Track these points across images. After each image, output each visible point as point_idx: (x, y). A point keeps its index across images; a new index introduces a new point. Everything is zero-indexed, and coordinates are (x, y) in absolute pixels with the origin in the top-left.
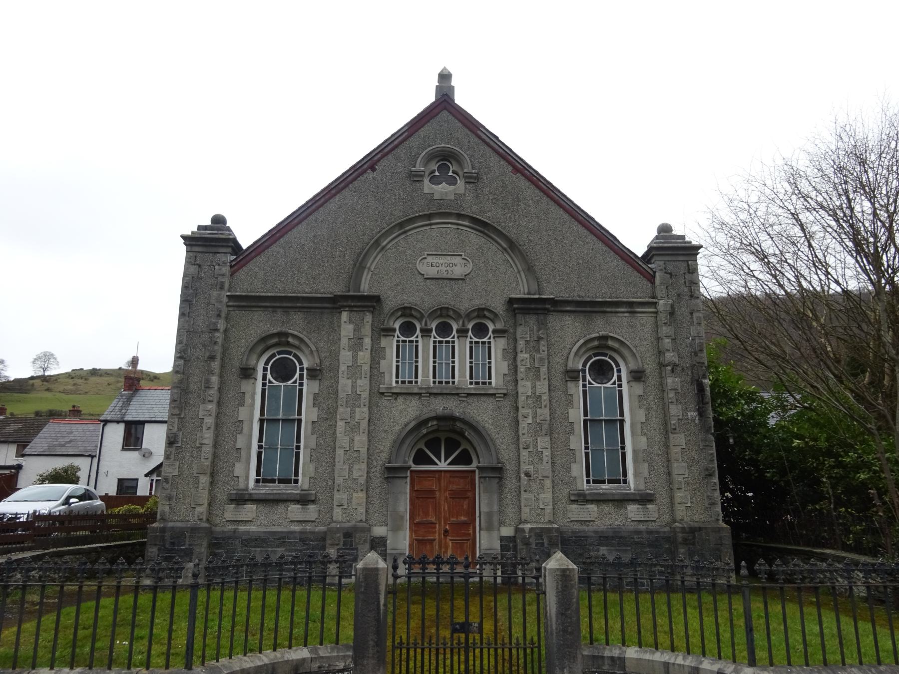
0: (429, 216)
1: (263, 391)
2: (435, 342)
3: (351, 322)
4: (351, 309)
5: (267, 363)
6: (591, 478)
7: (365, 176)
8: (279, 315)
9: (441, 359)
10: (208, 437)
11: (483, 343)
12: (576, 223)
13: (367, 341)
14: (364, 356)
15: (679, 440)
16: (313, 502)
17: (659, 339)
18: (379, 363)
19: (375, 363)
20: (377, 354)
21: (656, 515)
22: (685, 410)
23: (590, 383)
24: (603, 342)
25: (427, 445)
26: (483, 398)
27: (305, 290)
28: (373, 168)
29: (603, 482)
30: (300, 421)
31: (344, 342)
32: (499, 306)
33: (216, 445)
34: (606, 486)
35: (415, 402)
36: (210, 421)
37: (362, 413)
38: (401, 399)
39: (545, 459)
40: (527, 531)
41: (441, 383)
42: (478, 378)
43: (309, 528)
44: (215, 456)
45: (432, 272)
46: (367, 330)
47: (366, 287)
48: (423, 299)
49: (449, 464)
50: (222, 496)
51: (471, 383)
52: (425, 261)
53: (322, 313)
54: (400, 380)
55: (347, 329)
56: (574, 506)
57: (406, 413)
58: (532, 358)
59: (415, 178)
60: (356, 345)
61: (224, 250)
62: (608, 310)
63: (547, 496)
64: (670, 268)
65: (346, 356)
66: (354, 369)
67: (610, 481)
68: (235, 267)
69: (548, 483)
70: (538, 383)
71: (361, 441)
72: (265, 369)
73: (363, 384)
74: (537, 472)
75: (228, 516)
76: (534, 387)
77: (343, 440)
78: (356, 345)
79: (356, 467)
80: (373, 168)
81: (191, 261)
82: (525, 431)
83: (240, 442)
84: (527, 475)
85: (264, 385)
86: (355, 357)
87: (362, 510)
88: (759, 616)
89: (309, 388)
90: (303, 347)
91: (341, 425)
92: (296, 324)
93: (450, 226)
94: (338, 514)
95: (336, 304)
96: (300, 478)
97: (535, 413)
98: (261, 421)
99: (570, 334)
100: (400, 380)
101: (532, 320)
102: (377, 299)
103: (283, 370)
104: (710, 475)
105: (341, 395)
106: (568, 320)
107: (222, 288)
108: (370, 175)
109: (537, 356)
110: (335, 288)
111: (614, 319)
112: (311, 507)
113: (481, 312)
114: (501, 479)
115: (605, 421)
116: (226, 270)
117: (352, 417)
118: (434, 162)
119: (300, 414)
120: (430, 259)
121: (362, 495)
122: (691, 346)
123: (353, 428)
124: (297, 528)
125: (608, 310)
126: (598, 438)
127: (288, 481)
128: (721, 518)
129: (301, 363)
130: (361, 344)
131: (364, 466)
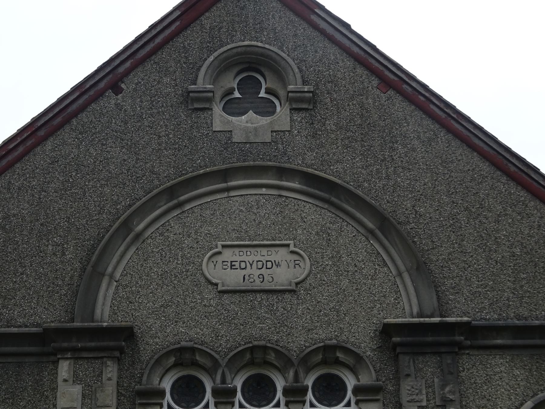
0: (225, 174)
3: (76, 379)
7: (102, 102)
12: (504, 179)
28: (116, 89)
45: (232, 279)
47: (105, 310)
52: (220, 259)
80: (116, 89)
93: (264, 191)
106: (499, 364)
108: (110, 101)
110: (47, 315)
113: (330, 354)
120: (228, 255)
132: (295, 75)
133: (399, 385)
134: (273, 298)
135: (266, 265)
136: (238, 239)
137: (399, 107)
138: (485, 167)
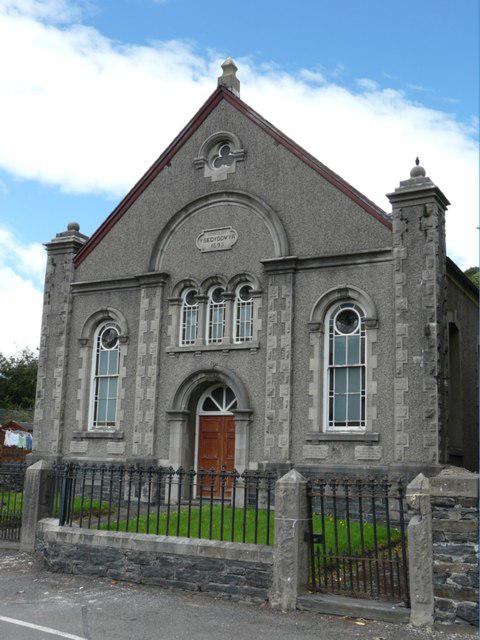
0: (206, 198)
1: (331, 342)
2: (211, 307)
3: (148, 297)
4: (149, 286)
5: (332, 317)
6: (333, 421)
7: (164, 171)
8: (104, 296)
9: (243, 319)
10: (58, 392)
11: (249, 304)
12: (327, 183)
13: (158, 311)
14: (155, 324)
15: (402, 384)
16: (376, 442)
17: (71, 312)
18: (167, 329)
19: (162, 329)
20: (164, 320)
21: (380, 455)
22: (410, 355)
23: (336, 334)
24: (344, 294)
25: (213, 394)
26: (241, 353)
27: (119, 274)
28: (168, 164)
29: (344, 424)
30: (363, 368)
31: (142, 312)
32: (257, 270)
33: (64, 397)
34: (346, 429)
35: (190, 358)
36: (60, 380)
37: (153, 369)
38: (181, 356)
39: (285, 404)
40: (265, 466)
41: (215, 341)
42: (242, 335)
43: (119, 459)
44: (64, 405)
45: (207, 246)
46: (157, 301)
47: (160, 266)
48: (198, 271)
49: (222, 406)
50: (69, 434)
51: (237, 340)
52: (202, 238)
53: (131, 292)
54: (186, 341)
55: (144, 303)
56: (309, 446)
57: (183, 368)
58: (279, 314)
59: (199, 166)
60: (150, 315)
61: (69, 251)
62: (360, 261)
63: (285, 437)
64: (406, 214)
65: (143, 324)
66: (148, 334)
67: (350, 424)
68: (77, 262)
69: (286, 425)
70: (282, 337)
71: (151, 391)
72: (331, 322)
73: (154, 346)
74: (277, 416)
75: (72, 449)
76: (279, 340)
77: (139, 391)
78: (150, 315)
79: (147, 413)
80: (168, 164)
81: (52, 263)
82: (270, 380)
83: (313, 390)
84: (270, 418)
85: (331, 336)
86: (149, 325)
87: (151, 445)
88: (227, 530)
89: (370, 337)
90: (360, 299)
91: (138, 379)
92: (113, 303)
93: (222, 203)
94: (135, 449)
95: (138, 281)
96: (366, 421)
97: (278, 363)
98: (331, 370)
99: (316, 285)
100: (186, 341)
101: (281, 279)
102: (166, 276)
103: (347, 320)
104: (430, 417)
105: (140, 356)
106: (314, 275)
107: (67, 280)
108: (167, 169)
109: (284, 312)
110: (139, 270)
111: (355, 271)
112: (121, 444)
113: (241, 278)
114: (250, 422)
115: (350, 368)
116: (70, 265)
117: (146, 373)
118: (216, 148)
119: (363, 362)
120: (206, 236)
121: (152, 434)
122: (422, 290)
123: (146, 382)
124: (365, 466)
125: (360, 261)
126: (342, 386)
127: (357, 424)
128: (437, 459)
129: (362, 314)
130: (153, 314)
131: (153, 412)
132: (372, 460)
133: (168, 438)
134: (222, 253)
135: (454, 316)
136: (216, 226)
137: (282, 151)
138: (318, 177)
